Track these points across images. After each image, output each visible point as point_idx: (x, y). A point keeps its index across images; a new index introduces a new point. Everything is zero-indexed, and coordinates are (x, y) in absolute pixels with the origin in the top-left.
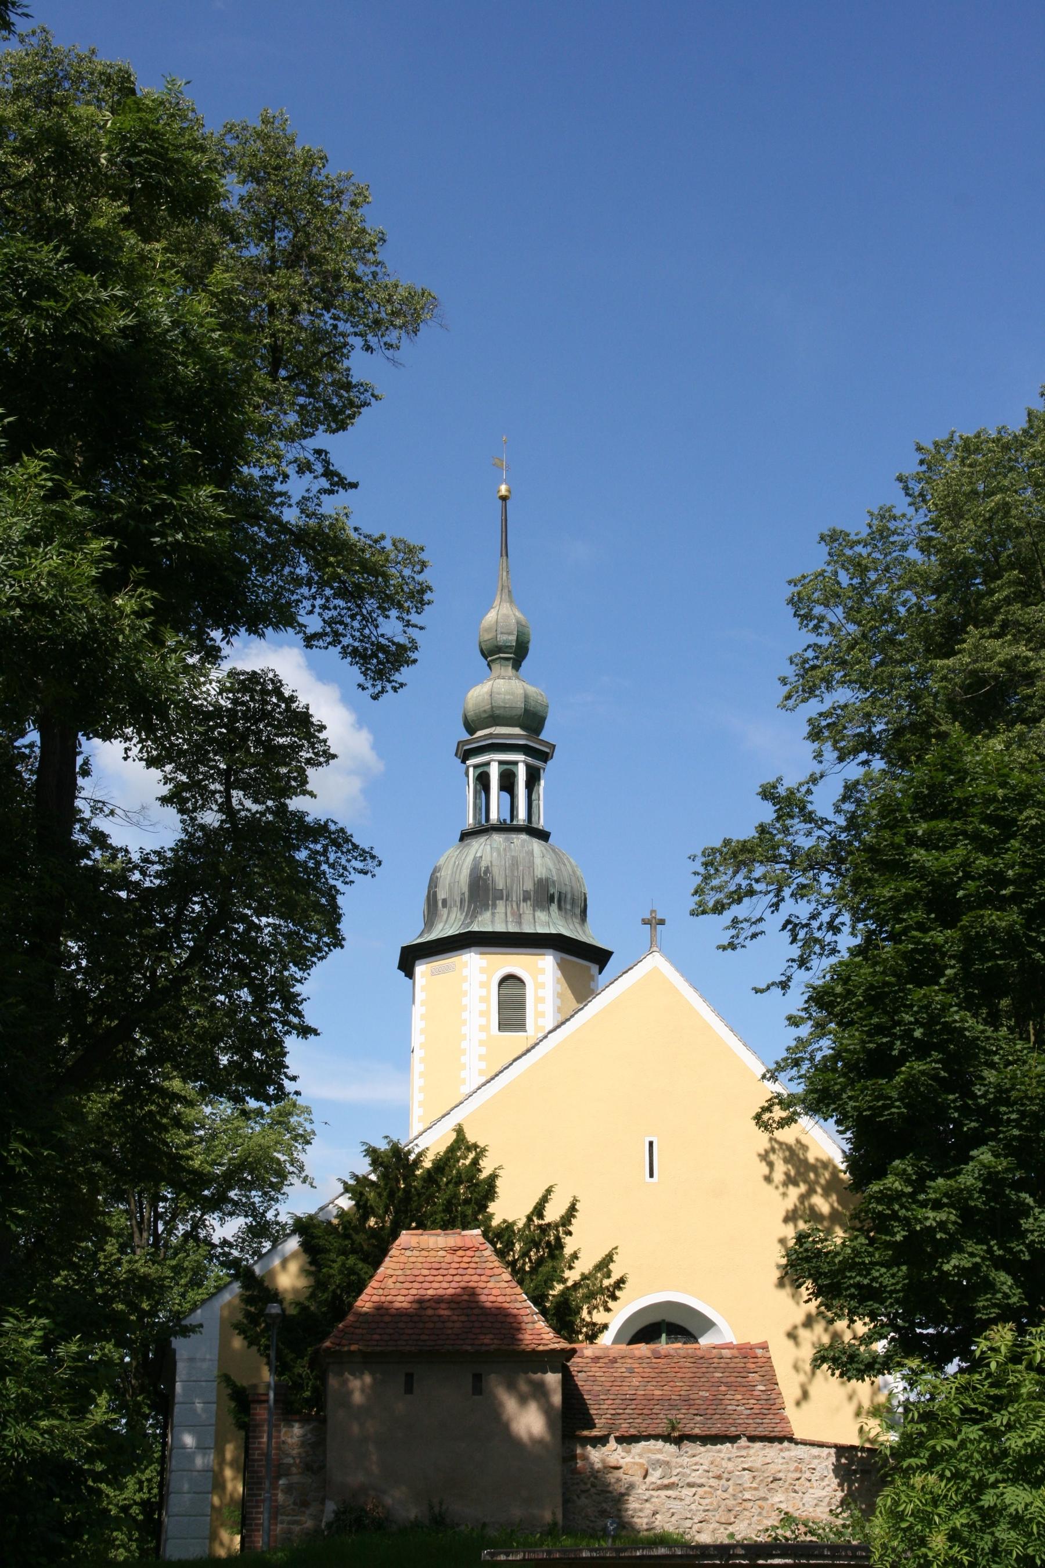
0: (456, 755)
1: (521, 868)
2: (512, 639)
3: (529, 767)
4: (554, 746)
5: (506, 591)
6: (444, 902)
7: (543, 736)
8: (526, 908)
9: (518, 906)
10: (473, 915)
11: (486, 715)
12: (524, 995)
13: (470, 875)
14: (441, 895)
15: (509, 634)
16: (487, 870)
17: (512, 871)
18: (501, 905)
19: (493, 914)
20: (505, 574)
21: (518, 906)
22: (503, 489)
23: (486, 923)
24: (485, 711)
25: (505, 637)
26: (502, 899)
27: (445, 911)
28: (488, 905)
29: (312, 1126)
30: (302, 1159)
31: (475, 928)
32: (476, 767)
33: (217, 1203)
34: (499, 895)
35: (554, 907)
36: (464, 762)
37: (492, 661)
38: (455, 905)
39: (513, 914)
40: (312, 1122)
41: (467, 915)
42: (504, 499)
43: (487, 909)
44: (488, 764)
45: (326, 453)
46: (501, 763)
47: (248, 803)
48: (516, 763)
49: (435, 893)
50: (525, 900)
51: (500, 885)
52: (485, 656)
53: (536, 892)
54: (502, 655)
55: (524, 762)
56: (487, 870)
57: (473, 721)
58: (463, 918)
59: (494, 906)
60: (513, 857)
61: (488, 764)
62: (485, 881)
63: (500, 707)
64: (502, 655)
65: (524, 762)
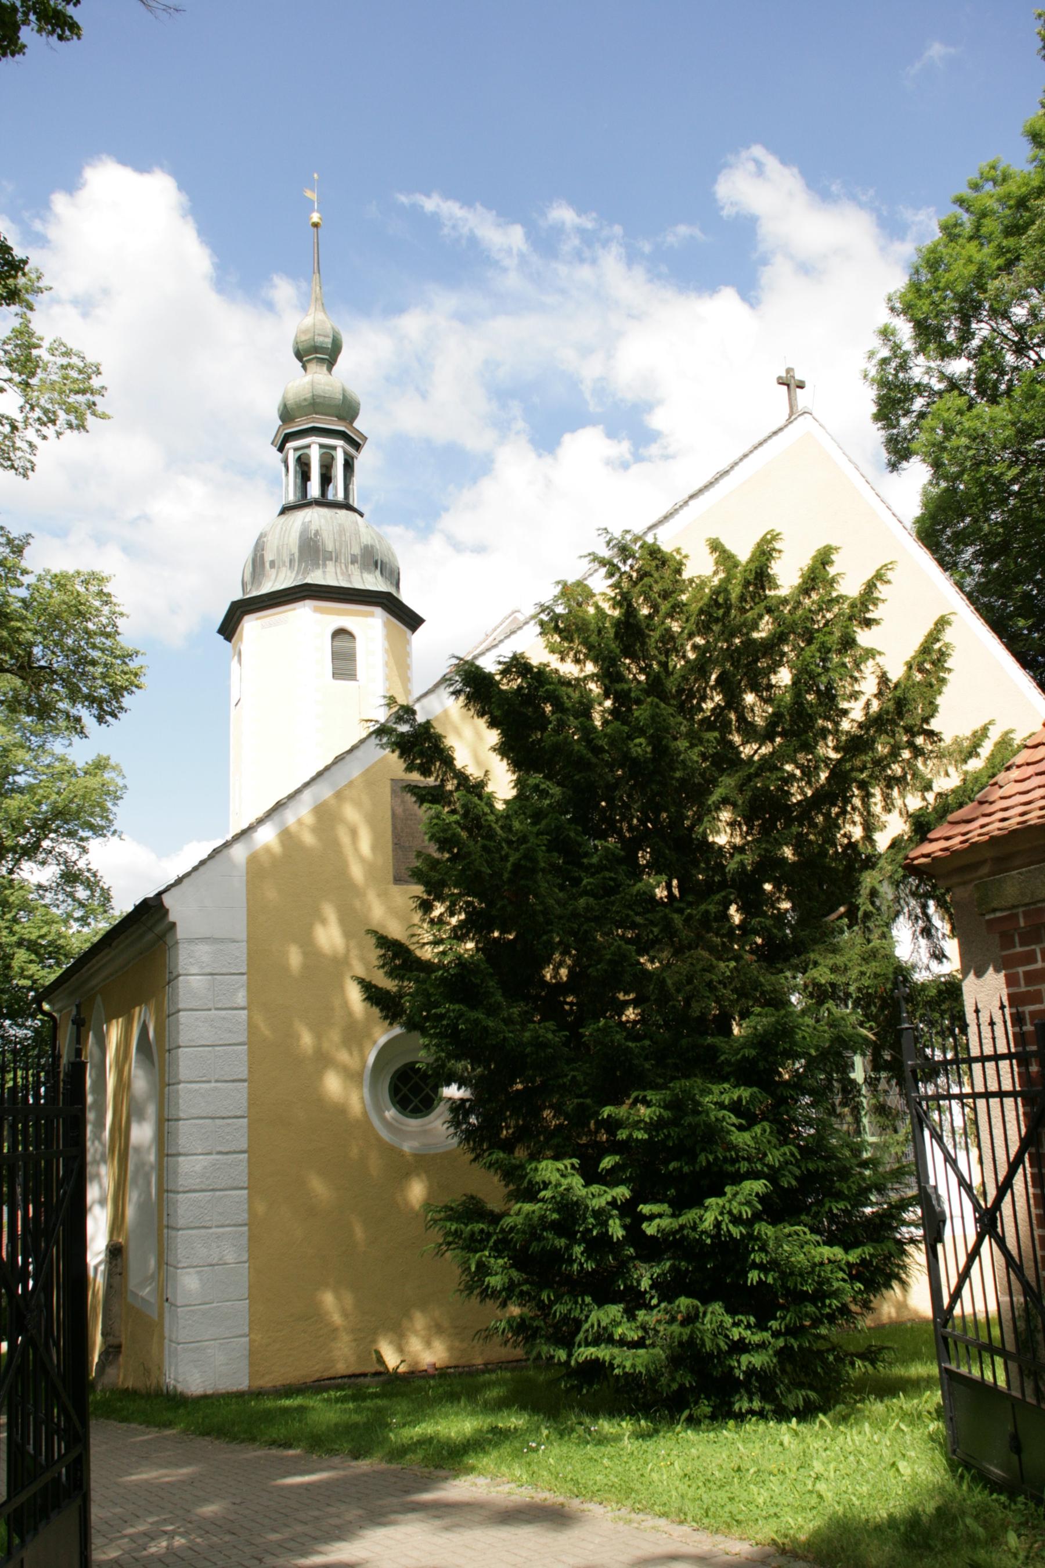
0: (272, 444)
1: (348, 534)
2: (328, 342)
3: (346, 453)
4: (366, 438)
5: (320, 302)
6: (272, 564)
7: (356, 424)
8: (354, 570)
9: (347, 567)
10: (306, 572)
11: (306, 403)
12: (354, 648)
13: (300, 537)
14: (269, 557)
15: (326, 336)
16: (317, 533)
17: (340, 536)
18: (330, 565)
19: (324, 572)
20: (318, 288)
21: (347, 567)
22: (315, 217)
23: (317, 577)
24: (305, 400)
25: (321, 339)
26: (331, 559)
27: (274, 571)
28: (318, 564)
29: (125, 782)
30: (541, 642)
31: (309, 580)
32: (296, 449)
33: (30, 852)
34: (328, 557)
35: (378, 572)
36: (281, 449)
37: (309, 361)
38: (284, 565)
39: (342, 574)
40: (124, 777)
41: (298, 573)
42: (316, 225)
43: (318, 567)
44: (308, 446)
45: (101, 580)
46: (322, 446)
47: (70, 852)
48: (334, 448)
49: (262, 556)
50: (353, 562)
51: (330, 547)
52: (299, 355)
53: (363, 556)
54: (319, 356)
55: (342, 447)
56: (317, 533)
57: (292, 409)
58: (293, 575)
59: (325, 565)
60: (340, 525)
61: (308, 446)
62: (316, 542)
63: (320, 396)
64: (319, 356)
65: (342, 447)
